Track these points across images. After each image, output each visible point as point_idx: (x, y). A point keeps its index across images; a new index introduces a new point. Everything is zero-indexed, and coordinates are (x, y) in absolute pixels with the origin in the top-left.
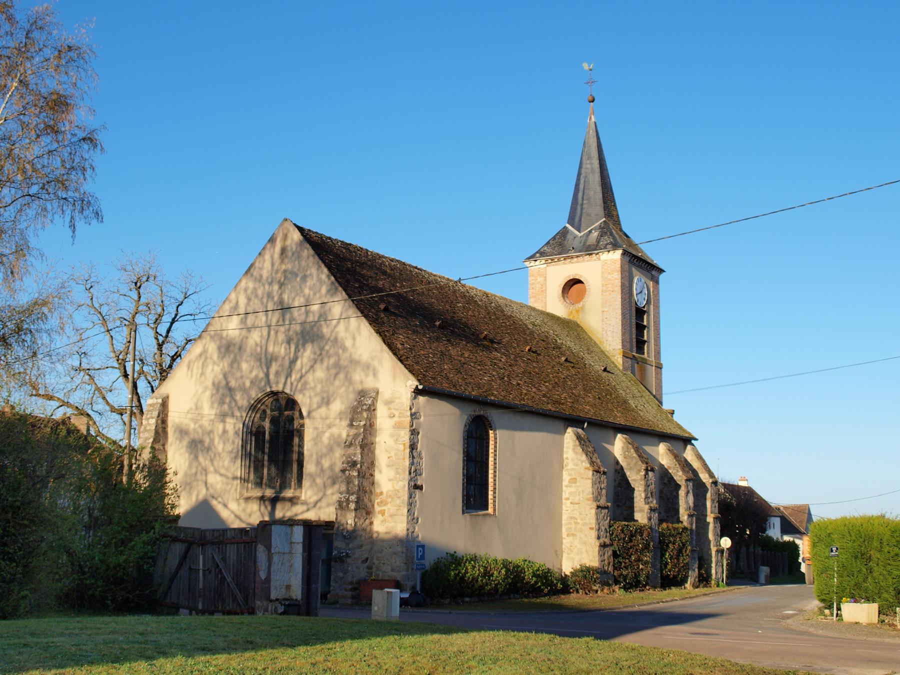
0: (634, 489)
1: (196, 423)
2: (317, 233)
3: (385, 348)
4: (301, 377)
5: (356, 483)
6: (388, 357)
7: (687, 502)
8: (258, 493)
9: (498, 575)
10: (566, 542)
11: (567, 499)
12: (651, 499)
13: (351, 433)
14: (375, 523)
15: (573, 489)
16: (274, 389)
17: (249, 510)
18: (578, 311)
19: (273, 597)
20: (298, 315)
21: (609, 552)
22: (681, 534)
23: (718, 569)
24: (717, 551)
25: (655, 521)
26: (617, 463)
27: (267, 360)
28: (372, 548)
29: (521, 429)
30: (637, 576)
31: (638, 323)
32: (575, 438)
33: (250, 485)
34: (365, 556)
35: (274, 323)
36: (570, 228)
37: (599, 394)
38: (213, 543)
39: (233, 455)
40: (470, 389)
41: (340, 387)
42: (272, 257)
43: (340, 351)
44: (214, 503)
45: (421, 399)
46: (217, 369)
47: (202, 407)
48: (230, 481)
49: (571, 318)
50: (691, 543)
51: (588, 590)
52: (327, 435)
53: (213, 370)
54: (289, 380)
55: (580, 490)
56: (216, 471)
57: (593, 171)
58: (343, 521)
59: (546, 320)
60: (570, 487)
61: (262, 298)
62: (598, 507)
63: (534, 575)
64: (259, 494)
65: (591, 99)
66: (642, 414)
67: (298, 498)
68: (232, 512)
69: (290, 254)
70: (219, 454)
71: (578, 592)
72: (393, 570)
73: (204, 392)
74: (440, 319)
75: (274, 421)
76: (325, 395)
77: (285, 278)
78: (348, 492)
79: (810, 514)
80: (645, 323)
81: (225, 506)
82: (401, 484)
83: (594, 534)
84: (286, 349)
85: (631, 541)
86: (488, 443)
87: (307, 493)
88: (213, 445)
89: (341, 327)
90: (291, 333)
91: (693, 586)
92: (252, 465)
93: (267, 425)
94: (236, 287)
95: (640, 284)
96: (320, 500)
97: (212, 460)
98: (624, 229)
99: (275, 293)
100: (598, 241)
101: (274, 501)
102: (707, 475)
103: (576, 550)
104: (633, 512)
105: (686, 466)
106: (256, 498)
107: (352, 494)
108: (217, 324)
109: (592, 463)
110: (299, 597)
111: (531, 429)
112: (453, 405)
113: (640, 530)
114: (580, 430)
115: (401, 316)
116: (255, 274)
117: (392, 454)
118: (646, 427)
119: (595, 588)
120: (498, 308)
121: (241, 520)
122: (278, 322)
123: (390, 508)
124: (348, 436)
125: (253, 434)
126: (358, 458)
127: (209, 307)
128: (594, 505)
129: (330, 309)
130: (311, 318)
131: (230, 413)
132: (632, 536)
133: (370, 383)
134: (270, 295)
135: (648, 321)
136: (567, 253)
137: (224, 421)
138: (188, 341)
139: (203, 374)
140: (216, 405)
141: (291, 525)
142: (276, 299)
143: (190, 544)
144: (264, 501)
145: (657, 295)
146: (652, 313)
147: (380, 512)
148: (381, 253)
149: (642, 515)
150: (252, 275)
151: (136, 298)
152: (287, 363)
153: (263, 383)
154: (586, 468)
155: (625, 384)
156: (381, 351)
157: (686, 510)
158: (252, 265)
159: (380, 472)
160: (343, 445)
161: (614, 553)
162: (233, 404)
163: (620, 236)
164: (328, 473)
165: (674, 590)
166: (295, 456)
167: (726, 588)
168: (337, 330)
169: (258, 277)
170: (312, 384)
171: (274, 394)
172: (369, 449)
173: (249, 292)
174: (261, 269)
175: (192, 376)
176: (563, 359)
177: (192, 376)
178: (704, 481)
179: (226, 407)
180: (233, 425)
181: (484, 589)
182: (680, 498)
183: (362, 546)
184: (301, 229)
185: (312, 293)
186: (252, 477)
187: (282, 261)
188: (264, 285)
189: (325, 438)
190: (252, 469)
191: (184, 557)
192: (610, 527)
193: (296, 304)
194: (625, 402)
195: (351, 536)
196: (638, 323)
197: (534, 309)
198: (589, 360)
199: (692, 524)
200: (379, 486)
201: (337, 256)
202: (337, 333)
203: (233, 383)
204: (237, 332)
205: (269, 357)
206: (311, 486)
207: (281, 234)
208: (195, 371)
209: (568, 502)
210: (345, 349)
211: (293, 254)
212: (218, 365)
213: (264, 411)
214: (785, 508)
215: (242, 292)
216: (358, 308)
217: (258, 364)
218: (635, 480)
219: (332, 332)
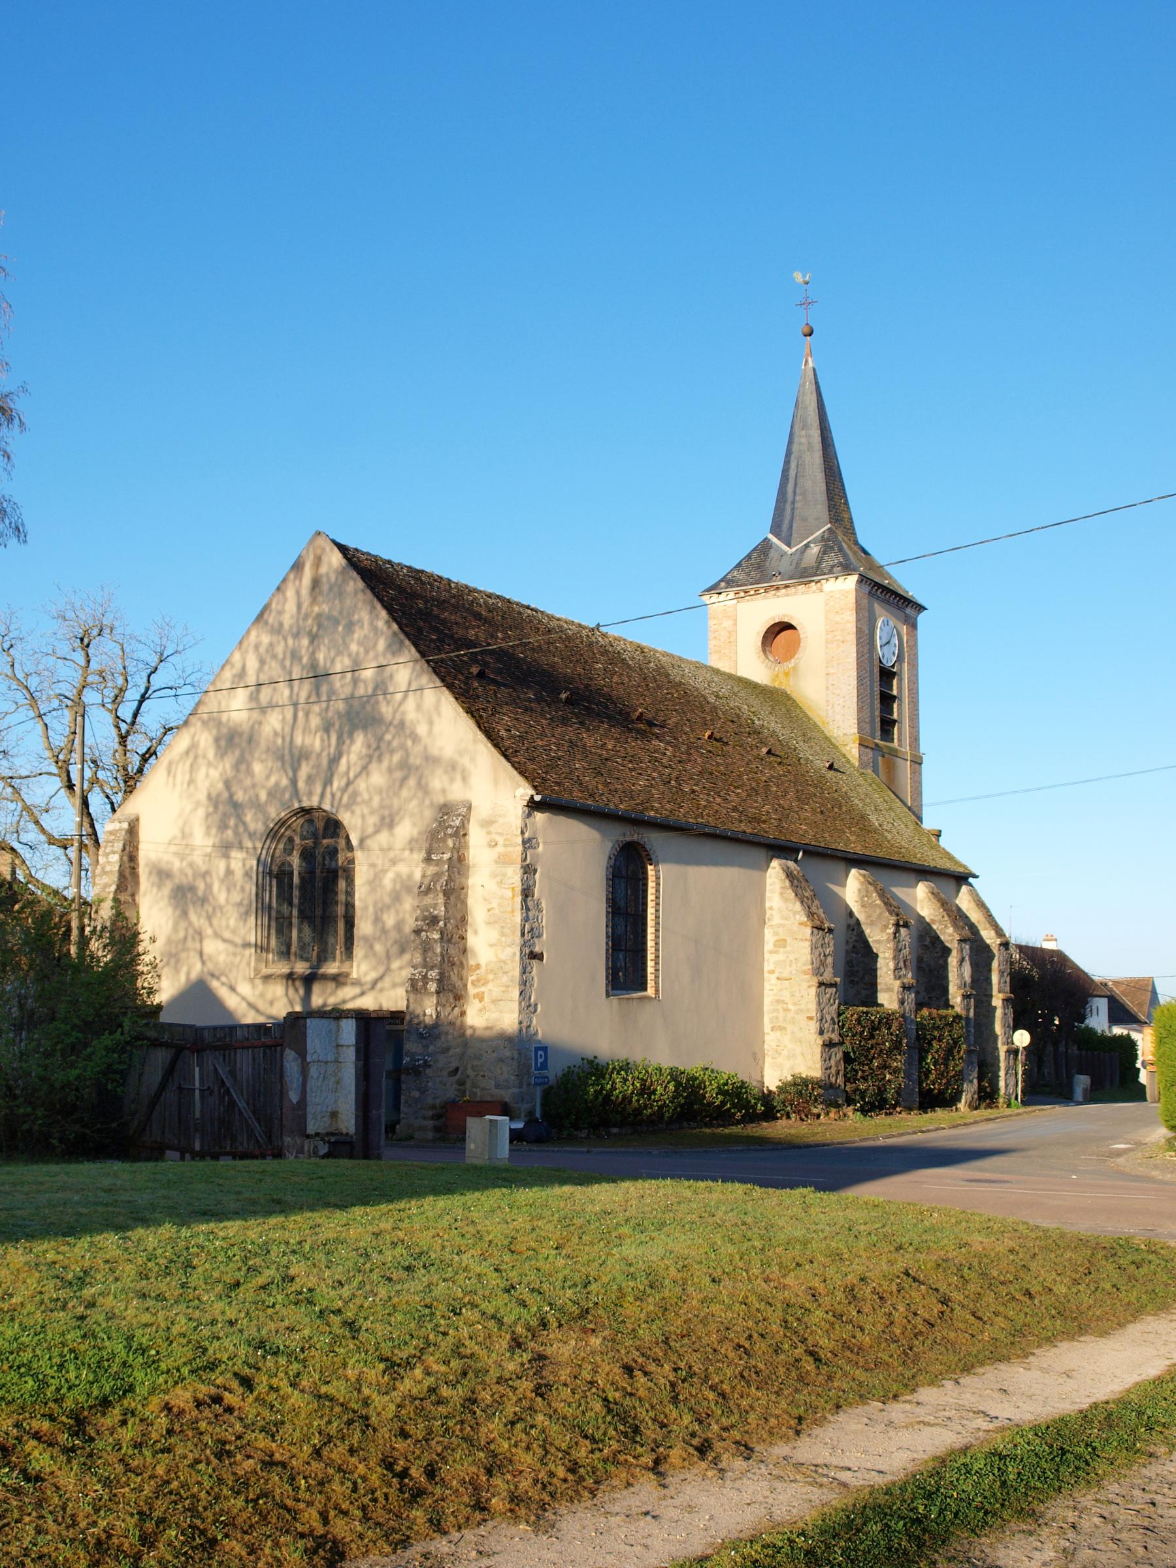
0: (877, 956)
1: (182, 860)
2: (368, 554)
3: (480, 736)
4: (348, 784)
5: (439, 950)
6: (485, 750)
7: (961, 976)
9: (663, 1092)
10: (771, 1039)
12: (903, 971)
13: (429, 873)
16: (306, 804)
17: (269, 996)
18: (787, 674)
19: (311, 1129)
21: (838, 1054)
22: (951, 1025)
23: (1009, 1079)
24: (1008, 1052)
25: (910, 1005)
26: (851, 914)
27: (291, 758)
28: (463, 1054)
30: (881, 1091)
31: (884, 693)
32: (783, 876)
33: (271, 956)
34: (454, 1065)
35: (302, 700)
36: (775, 540)
38: (215, 1048)
39: (243, 910)
40: (616, 800)
41: (410, 800)
42: (298, 593)
43: (409, 743)
44: (215, 984)
45: (540, 817)
46: (215, 774)
48: (239, 950)
49: (776, 685)
51: (804, 1114)
52: (390, 875)
53: (207, 775)
55: (792, 957)
56: (217, 935)
57: (810, 447)
58: (419, 1011)
59: (736, 689)
60: (776, 952)
61: (284, 659)
62: (821, 984)
63: (720, 1091)
64: (286, 970)
65: (807, 330)
66: (889, 837)
67: (347, 975)
68: (244, 998)
69: (325, 588)
71: (788, 1117)
72: (498, 1086)
73: (195, 810)
75: (307, 855)
76: (386, 813)
77: (320, 626)
78: (425, 965)
79: (1154, 992)
80: (895, 693)
81: (233, 989)
83: (814, 1026)
84: (322, 741)
85: (872, 1037)
86: (646, 885)
87: (361, 967)
88: (211, 892)
89: (411, 704)
90: (330, 714)
91: (969, 1106)
92: (273, 924)
93: (295, 861)
94: (241, 643)
95: (886, 629)
96: (381, 978)
97: (209, 918)
99: (303, 652)
100: (819, 561)
101: (309, 981)
102: (993, 933)
103: (785, 1052)
104: (876, 991)
105: (959, 918)
106: (281, 976)
108: (212, 703)
109: (811, 915)
110: (352, 1130)
111: (715, 863)
112: (589, 825)
113: (887, 1019)
114: (791, 864)
115: (505, 685)
116: (271, 621)
117: (495, 904)
119: (815, 1111)
120: (661, 670)
121: (257, 1010)
122: (309, 697)
123: (492, 989)
124: (424, 876)
125: (274, 875)
126: (441, 911)
127: (199, 675)
128: (814, 981)
129: (391, 676)
130: (361, 691)
131: (236, 842)
132: (874, 1028)
133: (457, 793)
134: (295, 656)
135: (900, 688)
137: (227, 856)
139: (191, 782)
140: (214, 831)
142: (305, 660)
143: (179, 1050)
144: (294, 980)
145: (914, 646)
147: (476, 996)
148: (472, 584)
150: (266, 623)
152: (325, 762)
153: (287, 796)
154: (801, 924)
156: (475, 741)
157: (959, 988)
158: (266, 608)
159: (476, 932)
160: (416, 891)
161: (846, 1055)
162: (241, 829)
163: (855, 553)
164: (394, 935)
165: (940, 1113)
166: (340, 910)
167: (1022, 1110)
168: (402, 708)
169: (276, 625)
170: (366, 796)
171: (305, 811)
172: (458, 898)
173: (262, 650)
174: (280, 613)
175: (174, 785)
176: (765, 750)
177: (174, 785)
178: (988, 942)
179: (230, 833)
180: (242, 863)
181: (641, 1113)
182: (950, 968)
183: (448, 1049)
184: (343, 549)
185: (362, 650)
186: (273, 942)
187: (314, 601)
188: (285, 639)
189: (388, 881)
190: (273, 931)
191: (170, 1071)
192: (839, 1015)
194: (863, 817)
195: (431, 1033)
196: (884, 693)
197: (717, 672)
198: (805, 751)
199: (968, 1010)
200: (475, 955)
201: (401, 590)
202: (404, 713)
203: (240, 796)
205: (296, 752)
206: (366, 956)
207: (311, 557)
208: (179, 777)
209: (773, 977)
210: (415, 738)
211: (331, 589)
212: (216, 768)
213: (291, 840)
214: (1116, 983)
215: (251, 650)
217: (279, 764)
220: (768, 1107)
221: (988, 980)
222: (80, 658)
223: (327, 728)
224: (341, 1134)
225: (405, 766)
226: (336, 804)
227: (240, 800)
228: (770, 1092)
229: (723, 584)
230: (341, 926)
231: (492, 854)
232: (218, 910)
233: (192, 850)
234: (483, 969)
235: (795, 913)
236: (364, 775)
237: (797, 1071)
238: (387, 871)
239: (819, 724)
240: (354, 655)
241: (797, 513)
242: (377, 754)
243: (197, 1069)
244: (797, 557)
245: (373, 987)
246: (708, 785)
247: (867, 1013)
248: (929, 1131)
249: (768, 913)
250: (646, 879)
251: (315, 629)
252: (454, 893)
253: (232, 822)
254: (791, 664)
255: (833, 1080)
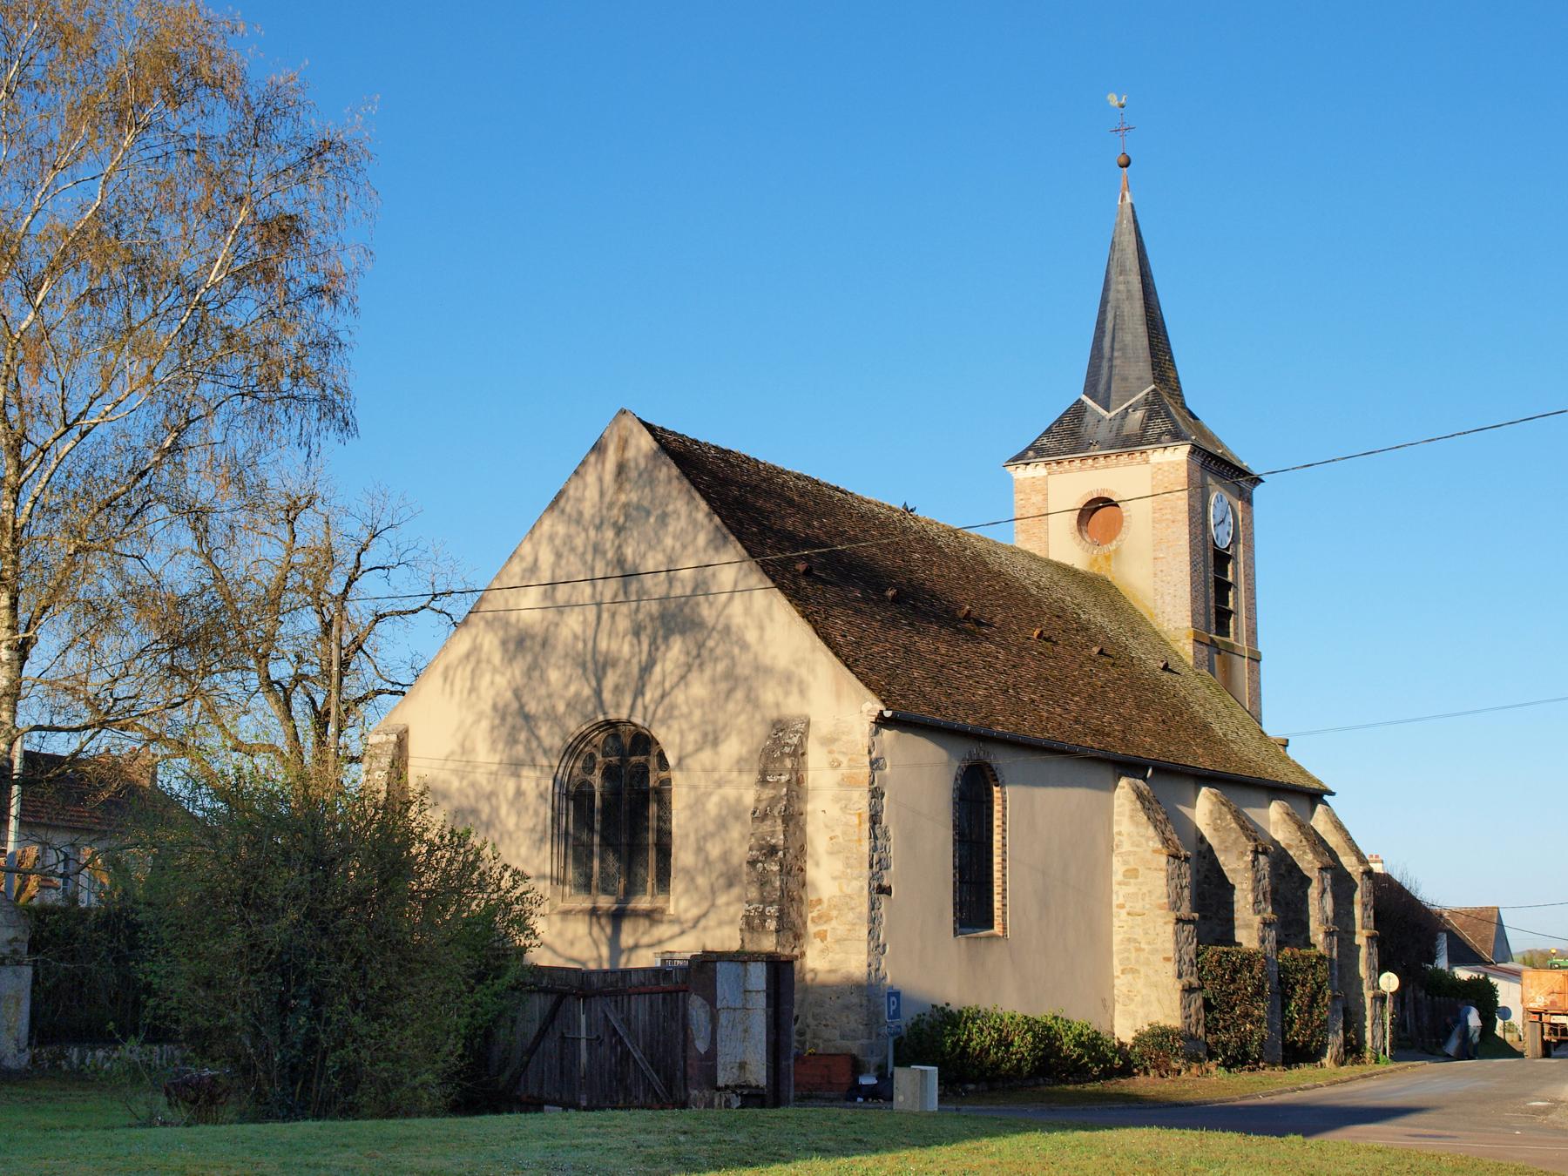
0: (1233, 887)
1: (462, 778)
2: (674, 433)
3: (819, 643)
4: (663, 697)
5: (778, 884)
6: (824, 659)
7: (1322, 909)
8: (583, 902)
9: (1022, 1044)
10: (1121, 983)
11: (1122, 906)
12: (1263, 905)
13: (764, 796)
14: (808, 953)
15: (1131, 889)
16: (612, 716)
19: (721, 1082)
20: (655, 586)
21: (1197, 1000)
22: (1314, 967)
23: (1376, 1030)
24: (1374, 998)
25: (1270, 944)
26: (1202, 839)
27: (597, 666)
29: (1043, 782)
31: (1218, 577)
32: (1134, 797)
33: (567, 889)
35: (607, 598)
36: (1089, 402)
37: (1163, 713)
38: (607, 994)
39: (537, 836)
40: (961, 713)
41: (738, 715)
42: (600, 480)
43: (736, 651)
45: (886, 734)
46: (502, 681)
47: (473, 750)
49: (1095, 570)
50: (1331, 987)
51: (1164, 1070)
52: (715, 799)
53: (492, 683)
54: (639, 701)
55: (1144, 890)
57: (1130, 297)
59: (1056, 578)
61: (584, 553)
62: (1179, 920)
64: (588, 905)
65: (1123, 160)
66: (1236, 748)
67: (662, 911)
69: (634, 474)
70: (510, 835)
71: (1147, 1073)
72: (843, 1037)
74: (893, 586)
75: (609, 773)
76: (709, 728)
77: (627, 516)
78: (763, 901)
79: (1500, 925)
80: (1230, 579)
82: (856, 884)
83: (1171, 968)
84: (632, 645)
85: (1233, 980)
86: (991, 809)
87: (679, 902)
88: (498, 816)
89: (737, 607)
90: (641, 616)
92: (570, 852)
93: (597, 780)
94: (532, 532)
96: (705, 915)
98: (1189, 405)
99: (608, 545)
100: (1144, 429)
101: (618, 917)
102: (1354, 859)
103: (1139, 998)
104: (1233, 928)
105: (1318, 843)
106: (581, 911)
107: (771, 904)
108: (496, 601)
109: (1166, 841)
110: (763, 1082)
113: (1249, 960)
114: (1140, 782)
115: (830, 583)
116: (568, 509)
117: (838, 832)
118: (1247, 773)
119: (1174, 1065)
120: (977, 556)
121: (554, 951)
122: (616, 595)
123: (836, 927)
124: (758, 800)
125: (573, 798)
126: (779, 839)
127: (415, 553)
128: (1172, 916)
129: (714, 575)
130: (677, 591)
131: (528, 760)
132: (1235, 971)
133: (792, 707)
134: (597, 549)
135: (1235, 573)
136: (1087, 450)
138: (379, 617)
139: (472, 690)
140: (500, 746)
141: (745, 962)
142: (610, 555)
143: (562, 996)
144: (599, 918)
145: (1249, 525)
146: (1241, 558)
147: (816, 935)
148: (779, 465)
149: (1249, 930)
150: (563, 511)
151: (287, 537)
152: (635, 670)
153: (590, 707)
154: (1155, 851)
155: (1198, 691)
156: (813, 650)
157: (1321, 924)
158: (561, 494)
159: (817, 864)
160: (749, 816)
161: (1206, 1002)
162: (534, 744)
163: (1184, 419)
164: (720, 867)
165: (1306, 1069)
166: (651, 838)
167: (1392, 1066)
168: (727, 612)
169: (574, 514)
170: (685, 709)
171: (609, 724)
173: (558, 542)
174: (580, 500)
175: (452, 693)
176: (1096, 650)
177: (452, 693)
178: (1349, 869)
180: (536, 783)
181: (998, 1067)
184: (650, 428)
185: (678, 545)
186: (570, 875)
187: (620, 489)
188: (586, 530)
189: (712, 805)
190: (570, 861)
191: (551, 1018)
192: (1198, 955)
193: (650, 565)
194: (1206, 726)
196: (1218, 577)
198: (1137, 651)
199: (1331, 950)
200: (815, 889)
201: (713, 474)
202: (729, 617)
203: (532, 707)
204: (537, 614)
205: (601, 659)
206: (687, 891)
207: (616, 439)
208: (457, 688)
209: (1123, 912)
210: (745, 646)
211: (640, 475)
212: (503, 674)
213: (592, 756)
214: (1453, 913)
215: (545, 542)
216: (766, 573)
217: (580, 671)
218: (1234, 871)
219: (718, 616)
220: (1121, 1062)
221: (1351, 914)
222: (284, 533)
223: (637, 632)
224: (749, 1087)
225: (732, 679)
226: (649, 717)
227: (533, 711)
228: (1122, 1044)
229: (1031, 453)
230: (652, 855)
231: (836, 776)
232: (506, 837)
233: (475, 767)
234: (825, 905)
235: (1148, 839)
236: (682, 685)
237: (1153, 1019)
238: (710, 794)
239: (1146, 615)
240: (669, 551)
241: (1116, 371)
242: (697, 662)
243: (583, 1018)
244: (1117, 423)
245: (694, 926)
246: (1045, 693)
247: (1227, 953)
248: (1306, 1089)
249: (1117, 838)
250: (991, 802)
251: (621, 520)
252: (793, 819)
253: (523, 736)
254: (1113, 546)
255: (1193, 1030)
